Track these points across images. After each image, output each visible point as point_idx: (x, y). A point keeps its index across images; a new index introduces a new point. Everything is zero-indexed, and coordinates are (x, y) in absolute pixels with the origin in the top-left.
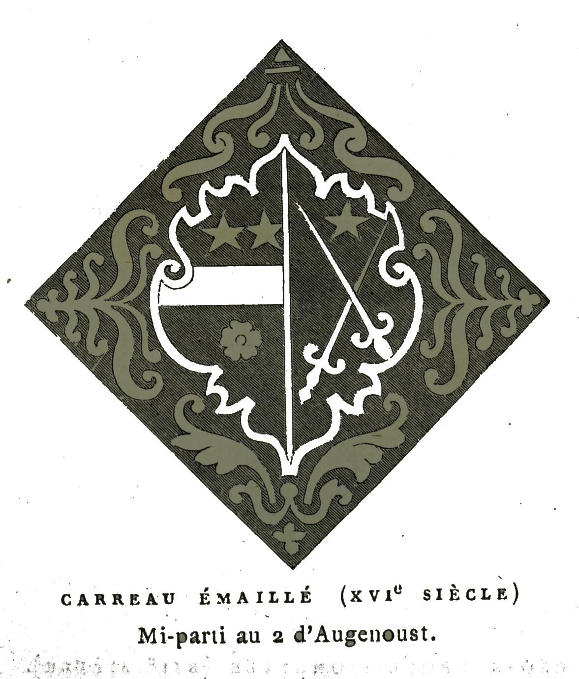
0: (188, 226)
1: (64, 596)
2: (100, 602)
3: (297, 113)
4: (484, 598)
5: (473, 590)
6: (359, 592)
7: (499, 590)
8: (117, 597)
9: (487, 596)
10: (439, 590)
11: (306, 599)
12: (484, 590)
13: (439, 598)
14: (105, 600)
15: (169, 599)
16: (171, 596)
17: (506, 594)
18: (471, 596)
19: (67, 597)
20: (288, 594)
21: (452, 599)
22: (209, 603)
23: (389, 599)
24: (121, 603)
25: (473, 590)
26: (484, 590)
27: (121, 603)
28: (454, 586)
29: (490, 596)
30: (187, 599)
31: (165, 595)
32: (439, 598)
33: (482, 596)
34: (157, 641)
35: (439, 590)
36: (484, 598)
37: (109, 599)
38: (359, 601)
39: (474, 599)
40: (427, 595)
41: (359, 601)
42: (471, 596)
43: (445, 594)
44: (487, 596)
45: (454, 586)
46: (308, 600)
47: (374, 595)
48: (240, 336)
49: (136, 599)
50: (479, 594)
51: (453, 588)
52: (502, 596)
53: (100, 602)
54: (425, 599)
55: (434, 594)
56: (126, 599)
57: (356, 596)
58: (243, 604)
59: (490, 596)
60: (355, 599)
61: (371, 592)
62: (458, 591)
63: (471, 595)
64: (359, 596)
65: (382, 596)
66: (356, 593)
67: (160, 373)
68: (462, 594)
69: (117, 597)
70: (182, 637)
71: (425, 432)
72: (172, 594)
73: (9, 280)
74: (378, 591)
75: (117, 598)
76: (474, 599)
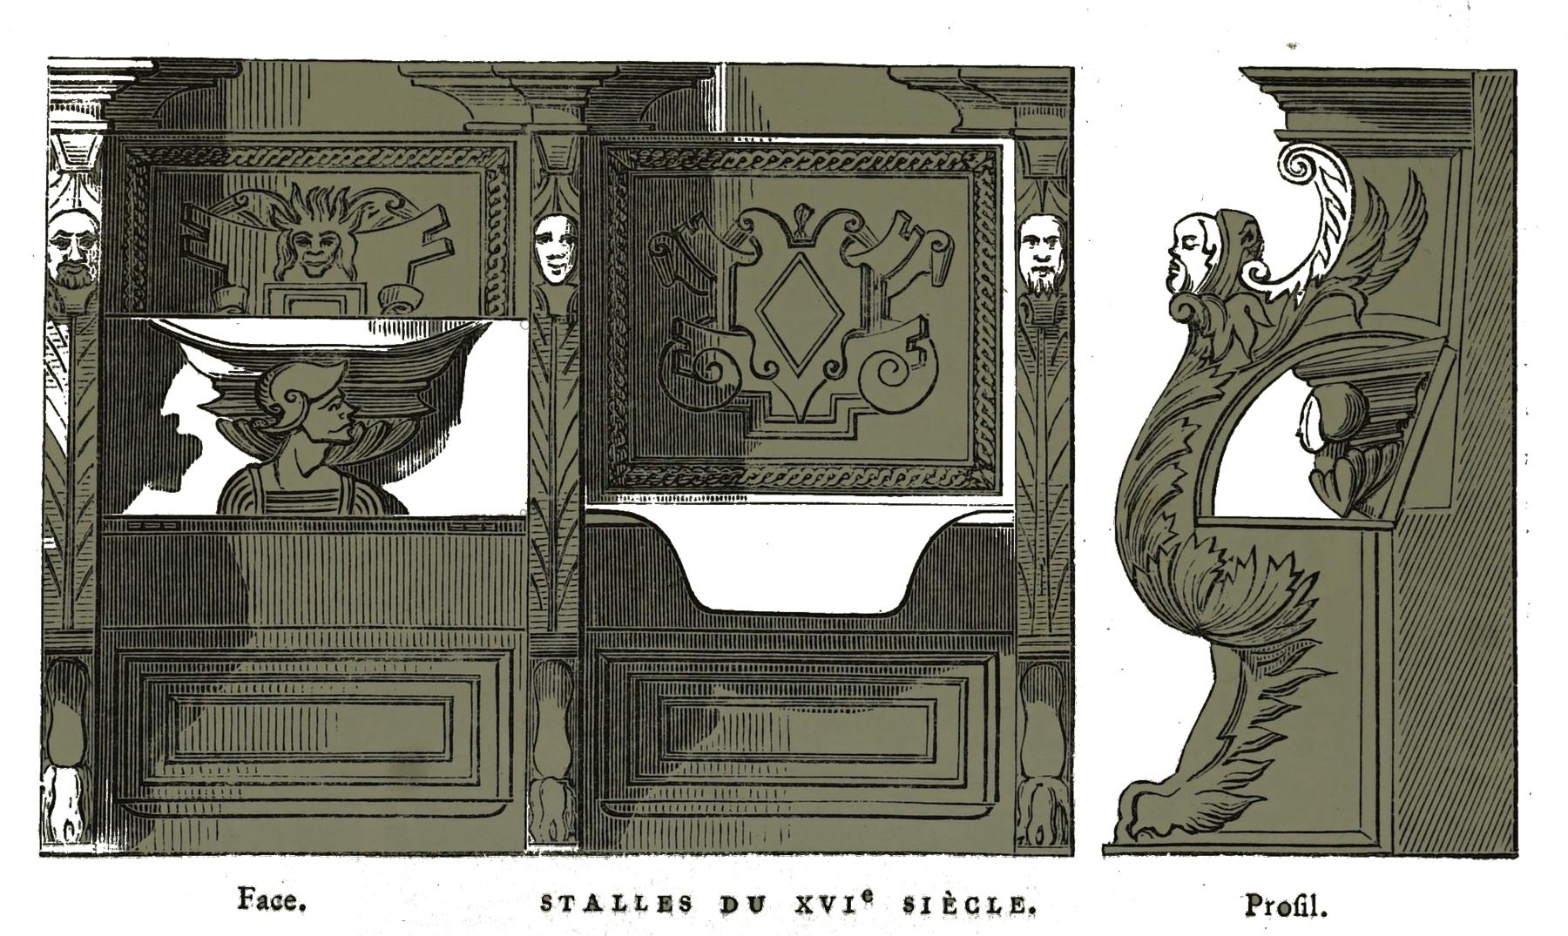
0: (1190, 330)
1: (972, 898)
3: (1203, 502)
4: (991, 911)
5: (976, 899)
6: (809, 898)
9: (643, 906)
10: (927, 900)
11: (1018, 908)
12: (992, 900)
13: (926, 911)
15: (757, 906)
16: (1317, 912)
19: (972, 902)
20: (618, 898)
21: (1013, 911)
22: (955, 912)
23: (849, 910)
26: (992, 900)
29: (1000, 909)
30: (780, 904)
31: (751, 899)
32: (926, 911)
33: (988, 908)
35: (927, 900)
36: (991, 911)
40: (909, 905)
43: (936, 905)
45: (948, 893)
46: (1020, 909)
49: (951, 905)
50: (984, 905)
51: (947, 896)
52: (1018, 908)
55: (919, 905)
57: (804, 905)
59: (1000, 909)
61: (823, 899)
63: (973, 906)
65: (840, 904)
68: (959, 905)
70: (1255, 900)
71: (245, 66)
72: (1313, 896)
73: (1291, 46)
74: (833, 898)
76: (977, 910)
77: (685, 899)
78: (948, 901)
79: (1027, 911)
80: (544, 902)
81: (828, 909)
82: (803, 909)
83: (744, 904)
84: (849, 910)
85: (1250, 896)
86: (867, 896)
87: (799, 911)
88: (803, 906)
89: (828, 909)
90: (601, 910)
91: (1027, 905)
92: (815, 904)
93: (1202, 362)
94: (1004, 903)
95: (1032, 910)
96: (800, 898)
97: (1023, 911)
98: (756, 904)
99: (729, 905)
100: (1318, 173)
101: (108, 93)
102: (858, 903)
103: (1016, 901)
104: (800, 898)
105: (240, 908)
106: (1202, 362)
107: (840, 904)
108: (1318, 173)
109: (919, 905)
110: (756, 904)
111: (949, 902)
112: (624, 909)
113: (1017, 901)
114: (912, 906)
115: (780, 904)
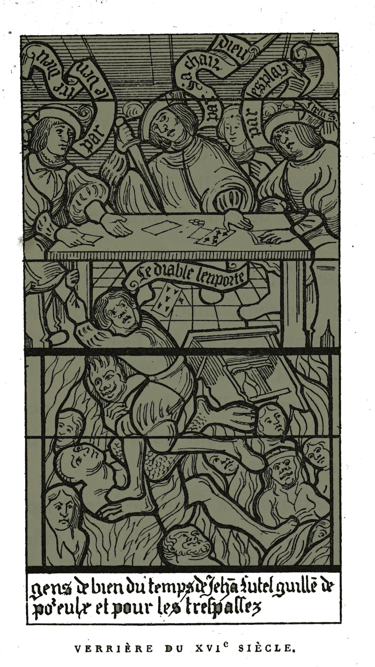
2: (138, 650)
4: (276, 650)
5: (270, 646)
6: (201, 645)
7: (86, 646)
8: (109, 647)
11: (88, 650)
12: (277, 646)
13: (249, 651)
14: (112, 649)
17: (91, 648)
18: (268, 649)
19: (268, 647)
22: (261, 651)
23: (218, 651)
24: (101, 651)
25: (270, 646)
26: (277, 646)
27: (101, 651)
28: (258, 643)
32: (249, 651)
33: (275, 649)
34: (75, 647)
36: (276, 650)
37: (104, 649)
38: (201, 651)
39: (270, 650)
40: (241, 648)
41: (201, 651)
42: (268, 649)
43: (253, 648)
44: (278, 649)
47: (78, 648)
48: (71, 497)
49: (89, 649)
50: (273, 648)
51: (257, 644)
52: (88, 650)
53: (109, 650)
54: (240, 650)
55: (246, 648)
56: (144, 649)
57: (199, 648)
58: (199, 653)
60: (199, 650)
61: (208, 646)
62: (260, 646)
63: (268, 648)
64: (201, 648)
65: (214, 649)
66: (199, 646)
67: (238, 496)
69: (138, 647)
72: (181, 646)
74: (80, 646)
75: (99, 648)
76: (270, 650)
77: (241, 646)
78: (88, 648)
79: (292, 651)
80: (240, 647)
81: (210, 650)
82: (199, 650)
83: (174, 649)
84: (218, 651)
85: (167, 646)
86: (225, 644)
87: (197, 651)
88: (199, 649)
89: (210, 650)
90: (202, 651)
91: (291, 648)
92: (204, 648)
93: (190, 510)
94: (282, 647)
95: (294, 651)
96: (197, 646)
97: (290, 650)
98: (179, 649)
99: (169, 649)
100: (274, 485)
101: (243, 84)
102: (221, 648)
103: (149, 648)
104: (197, 646)
105: (275, 651)
106: (190, 510)
107: (214, 649)
108: (274, 485)
109: (246, 648)
110: (179, 649)
111: (128, 647)
112: (280, 650)
113: (288, 646)
114: (242, 648)
115: (234, 647)
